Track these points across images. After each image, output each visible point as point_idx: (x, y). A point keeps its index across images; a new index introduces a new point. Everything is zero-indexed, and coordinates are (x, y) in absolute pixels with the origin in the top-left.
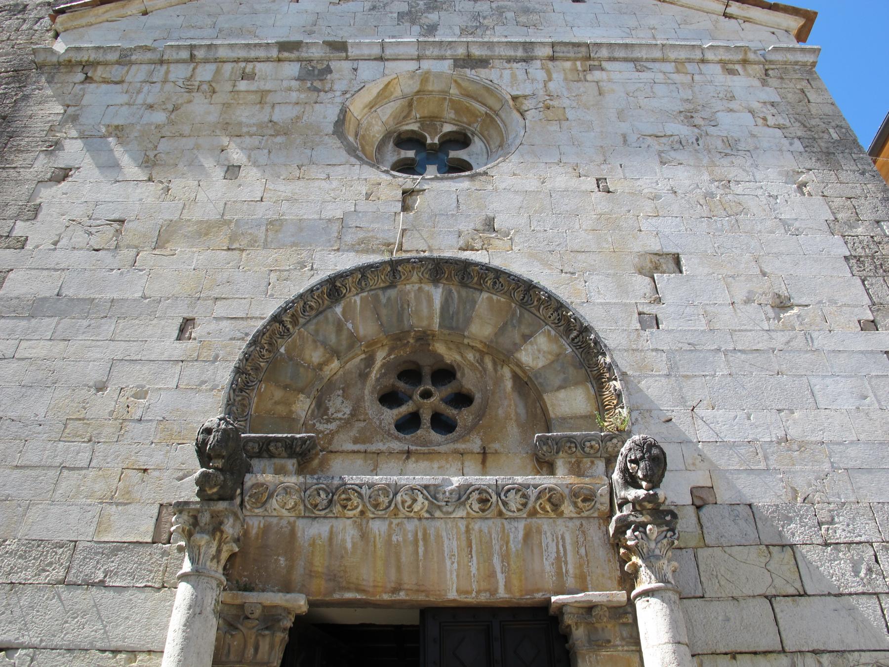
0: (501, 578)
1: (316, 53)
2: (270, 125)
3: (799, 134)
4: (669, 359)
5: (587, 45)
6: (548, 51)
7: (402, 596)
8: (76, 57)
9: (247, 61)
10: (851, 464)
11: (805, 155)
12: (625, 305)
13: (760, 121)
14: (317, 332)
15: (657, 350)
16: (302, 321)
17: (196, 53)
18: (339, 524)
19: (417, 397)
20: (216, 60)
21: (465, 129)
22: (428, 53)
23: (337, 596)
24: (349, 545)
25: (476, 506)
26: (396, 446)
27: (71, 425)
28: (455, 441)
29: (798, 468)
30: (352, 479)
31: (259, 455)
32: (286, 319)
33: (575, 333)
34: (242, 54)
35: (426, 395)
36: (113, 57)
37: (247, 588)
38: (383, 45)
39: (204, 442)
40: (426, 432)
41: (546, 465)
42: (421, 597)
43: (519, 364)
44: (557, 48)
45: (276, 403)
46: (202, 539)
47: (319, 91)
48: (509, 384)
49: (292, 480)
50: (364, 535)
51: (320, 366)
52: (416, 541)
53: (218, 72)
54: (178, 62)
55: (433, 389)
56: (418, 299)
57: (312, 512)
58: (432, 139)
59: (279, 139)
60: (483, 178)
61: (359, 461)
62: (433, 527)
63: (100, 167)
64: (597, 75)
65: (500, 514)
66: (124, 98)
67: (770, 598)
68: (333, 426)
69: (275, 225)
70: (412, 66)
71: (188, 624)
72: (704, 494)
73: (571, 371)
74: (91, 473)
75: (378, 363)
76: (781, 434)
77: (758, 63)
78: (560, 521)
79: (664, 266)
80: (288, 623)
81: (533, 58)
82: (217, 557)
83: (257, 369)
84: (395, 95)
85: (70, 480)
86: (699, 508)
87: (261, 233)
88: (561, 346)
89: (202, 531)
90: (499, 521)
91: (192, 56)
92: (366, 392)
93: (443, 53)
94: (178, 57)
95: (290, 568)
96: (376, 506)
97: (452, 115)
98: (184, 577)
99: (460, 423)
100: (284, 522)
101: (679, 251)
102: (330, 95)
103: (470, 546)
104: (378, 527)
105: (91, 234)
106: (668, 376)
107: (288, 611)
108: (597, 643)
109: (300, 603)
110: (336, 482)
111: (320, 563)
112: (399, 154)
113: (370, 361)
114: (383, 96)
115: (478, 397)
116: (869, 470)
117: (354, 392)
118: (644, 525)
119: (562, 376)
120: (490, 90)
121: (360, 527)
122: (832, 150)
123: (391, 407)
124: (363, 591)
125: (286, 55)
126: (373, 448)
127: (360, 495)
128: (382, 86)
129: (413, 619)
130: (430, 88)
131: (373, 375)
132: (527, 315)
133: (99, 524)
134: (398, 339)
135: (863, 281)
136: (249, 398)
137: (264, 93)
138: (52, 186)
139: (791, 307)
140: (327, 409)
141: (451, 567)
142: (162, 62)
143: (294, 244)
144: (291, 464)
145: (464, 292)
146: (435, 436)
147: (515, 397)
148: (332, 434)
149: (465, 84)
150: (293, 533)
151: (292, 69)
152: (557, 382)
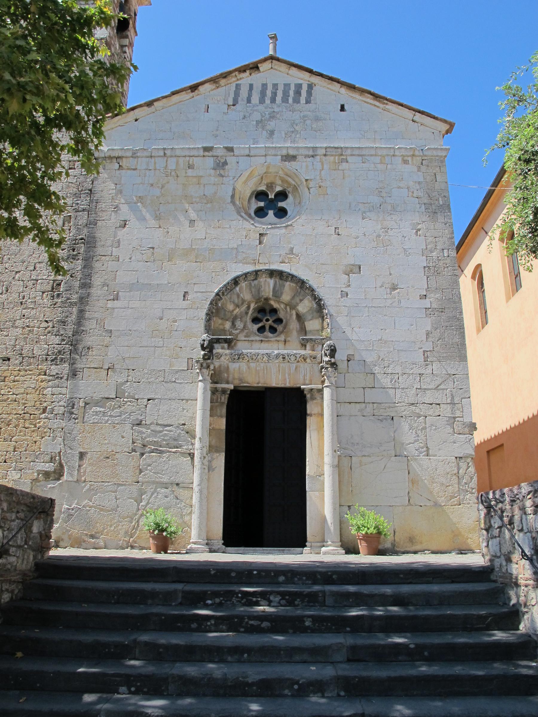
0: (288, 380)
2: (204, 197)
3: (425, 201)
4: (348, 310)
5: (342, 148)
6: (323, 151)
7: (260, 385)
8: (113, 154)
9: (190, 156)
10: (400, 348)
11: (425, 213)
12: (337, 287)
13: (410, 194)
14: (231, 298)
15: (345, 306)
16: (225, 294)
17: (166, 152)
18: (242, 364)
19: (264, 321)
20: (176, 156)
21: (285, 189)
22: (270, 153)
23: (242, 385)
24: (245, 371)
25: (282, 359)
26: (258, 338)
27: (154, 332)
28: (276, 337)
29: (382, 349)
30: (245, 351)
31: (216, 343)
32: (220, 294)
33: (317, 300)
34: (187, 153)
35: (267, 320)
36: (129, 154)
38: (250, 148)
39: (203, 344)
41: (304, 346)
42: (265, 385)
43: (298, 310)
44: (328, 150)
45: (220, 325)
46: (204, 371)
47: (223, 176)
48: (294, 317)
49: (227, 352)
50: (249, 368)
51: (233, 311)
52: (264, 370)
53: (177, 163)
54: (159, 156)
55: (269, 318)
56: (265, 284)
57: (233, 360)
58: (271, 195)
59: (209, 205)
60: (290, 227)
62: (269, 365)
64: (344, 165)
65: (289, 362)
67: (364, 388)
68: (238, 331)
70: (262, 160)
73: (315, 314)
74: (165, 348)
76: (380, 338)
77: (420, 156)
78: (306, 364)
79: (354, 270)
80: (229, 392)
82: (208, 375)
83: (212, 313)
84: (255, 175)
86: (349, 361)
88: (312, 304)
89: (204, 368)
90: (288, 363)
91: (165, 154)
92: (248, 319)
94: (159, 155)
95: (228, 377)
96: (252, 359)
98: (200, 381)
99: (278, 330)
100: (225, 364)
101: (361, 264)
103: (279, 371)
104: (253, 365)
105: (143, 254)
107: (228, 389)
108: (313, 398)
109: (232, 387)
110: (240, 352)
111: (236, 376)
112: (257, 204)
113: (249, 308)
115: (284, 320)
116: (405, 351)
117: (244, 319)
118: (328, 368)
119: (312, 316)
121: (248, 365)
122: (437, 211)
123: (256, 324)
124: (249, 384)
125: (207, 154)
126: (250, 339)
127: (248, 356)
128: (249, 172)
129: (264, 390)
130: (271, 171)
132: (302, 292)
133: (170, 364)
134: (258, 301)
135: (427, 278)
136: (211, 323)
138: (121, 230)
139: (397, 289)
140: (235, 325)
144: (226, 345)
145: (281, 282)
146: (270, 335)
147: (296, 321)
148: (238, 334)
149: (285, 170)
150: (228, 367)
151: (210, 162)
152: (310, 317)
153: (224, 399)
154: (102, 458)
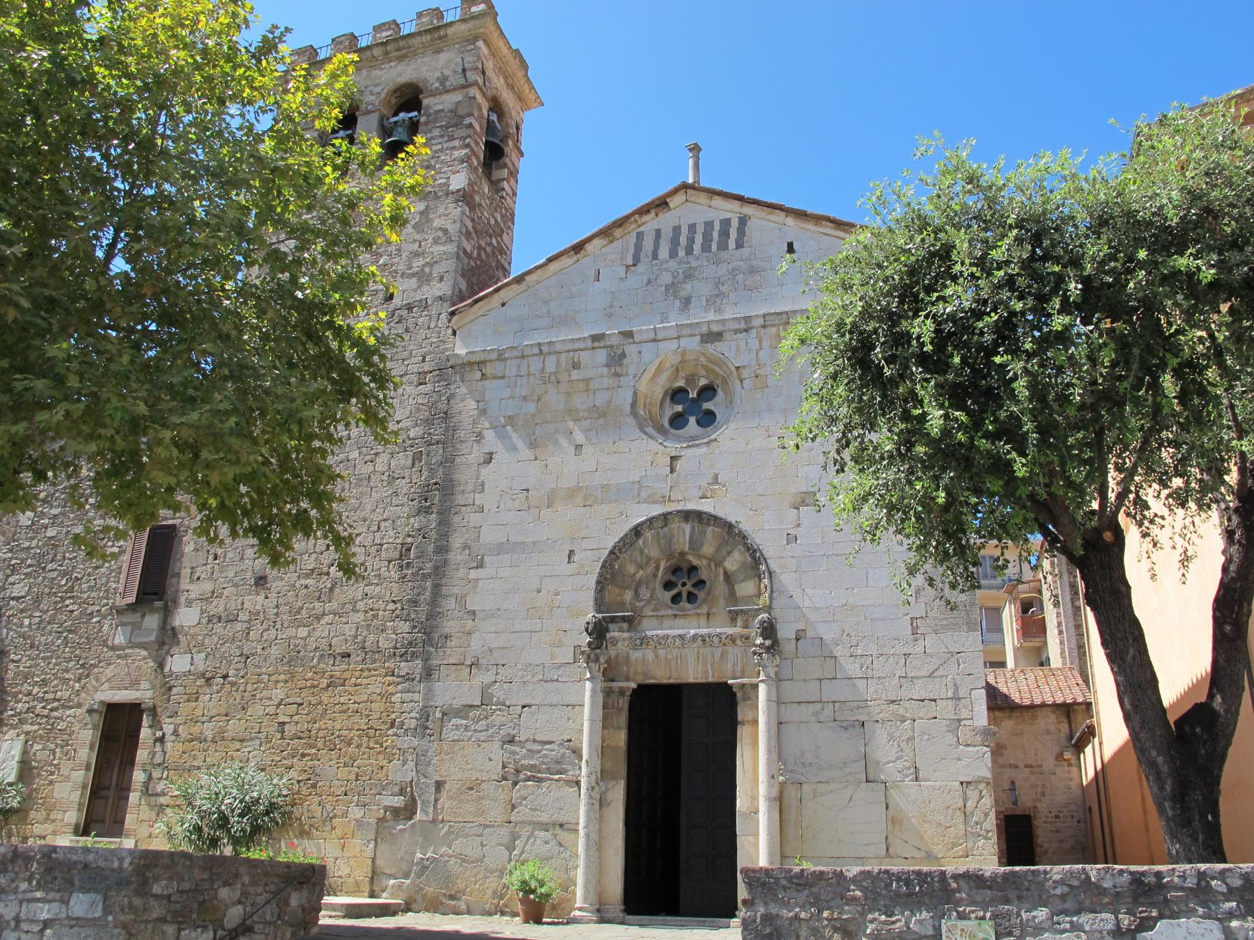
1: (614, 341)
8: (474, 358)
18: (646, 652)
22: (684, 333)
26: (670, 612)
31: (612, 622)
32: (616, 551)
34: (570, 346)
35: (684, 584)
36: (494, 356)
37: (612, 680)
38: (655, 329)
40: (684, 604)
44: (767, 318)
46: (592, 665)
48: (721, 577)
50: (657, 656)
51: (634, 575)
54: (533, 355)
57: (635, 647)
59: (601, 421)
61: (654, 620)
63: (507, 450)
66: (507, 393)
67: (820, 680)
69: (605, 488)
71: (592, 697)
72: (801, 633)
75: (661, 569)
76: (844, 602)
81: (751, 328)
83: (606, 579)
85: (536, 636)
87: (599, 493)
93: (693, 332)
95: (628, 671)
97: (704, 373)
98: (588, 679)
102: (626, 379)
104: (662, 652)
106: (795, 571)
108: (746, 698)
109: (634, 685)
111: (639, 669)
113: (657, 568)
114: (659, 370)
116: (883, 620)
120: (720, 363)
125: (596, 344)
131: (660, 574)
134: (670, 556)
137: (587, 381)
141: (691, 668)
142: (523, 357)
143: (617, 501)
145: (701, 526)
146: (688, 606)
148: (643, 607)
150: (628, 656)
153: (624, 703)
154: (463, 789)
